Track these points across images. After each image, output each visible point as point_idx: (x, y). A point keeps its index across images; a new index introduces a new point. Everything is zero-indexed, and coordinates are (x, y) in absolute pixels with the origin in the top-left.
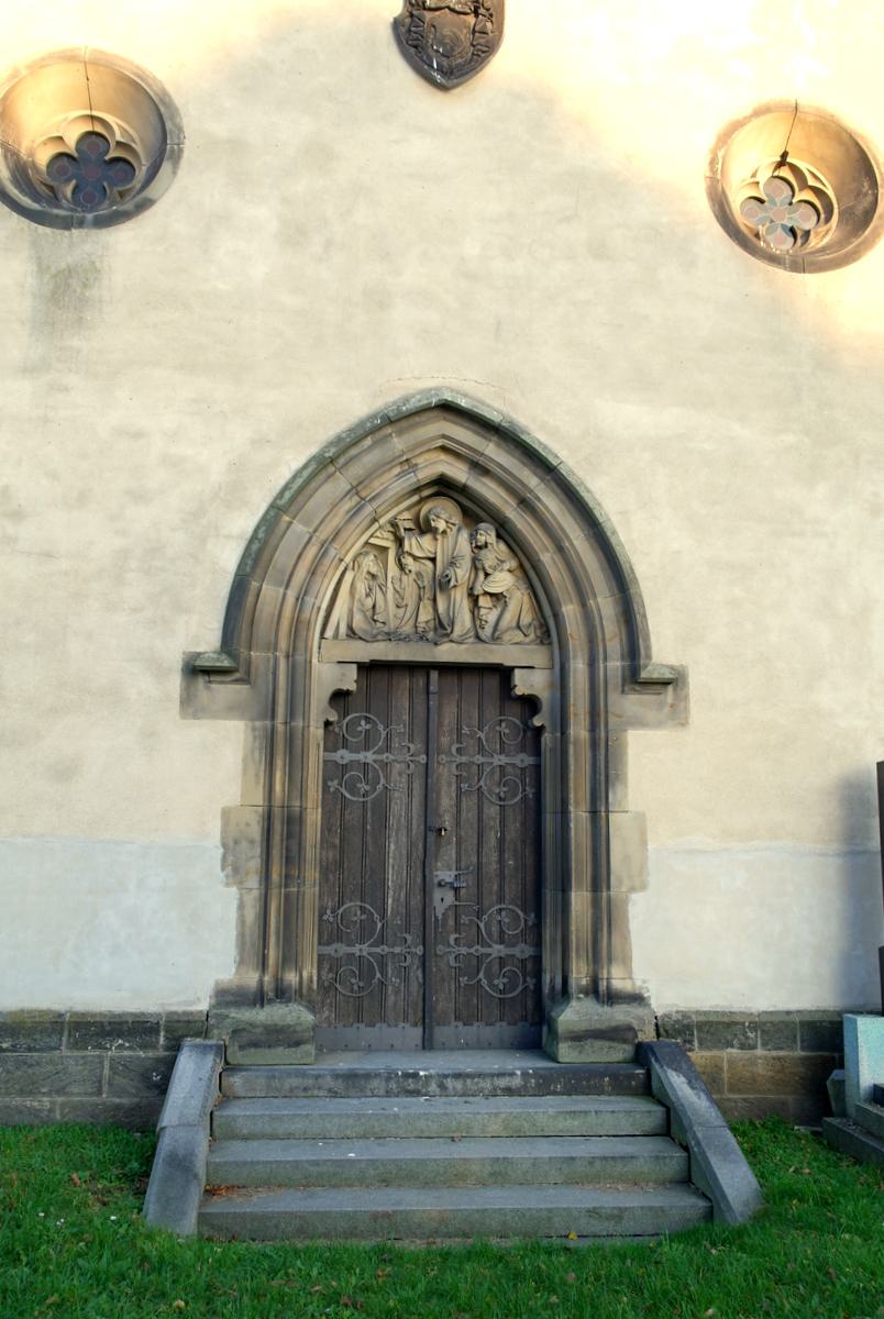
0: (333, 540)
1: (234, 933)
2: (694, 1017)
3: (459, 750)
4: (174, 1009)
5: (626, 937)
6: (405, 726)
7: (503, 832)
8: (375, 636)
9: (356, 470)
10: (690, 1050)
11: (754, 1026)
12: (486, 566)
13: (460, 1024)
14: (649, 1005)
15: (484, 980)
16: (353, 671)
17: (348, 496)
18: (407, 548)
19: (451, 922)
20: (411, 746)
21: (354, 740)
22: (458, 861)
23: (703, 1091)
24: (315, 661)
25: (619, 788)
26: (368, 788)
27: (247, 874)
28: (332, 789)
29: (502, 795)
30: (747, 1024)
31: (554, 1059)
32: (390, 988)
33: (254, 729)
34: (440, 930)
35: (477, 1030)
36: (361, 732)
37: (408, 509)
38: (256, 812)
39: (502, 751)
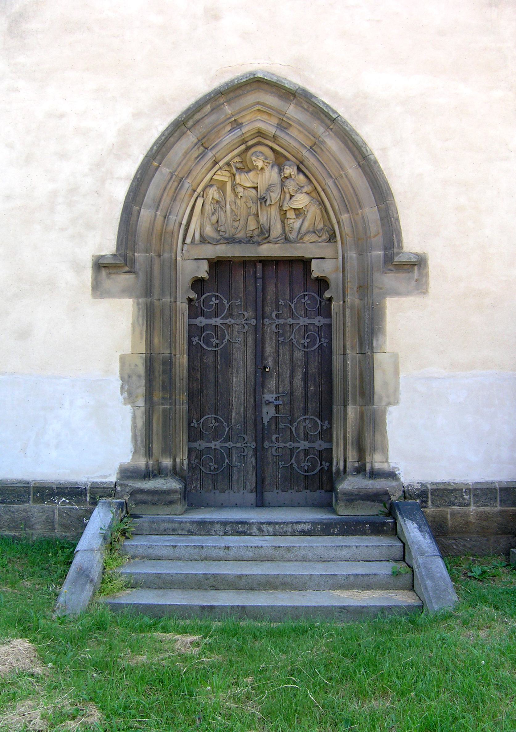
0: (187, 177)
1: (130, 434)
2: (428, 486)
3: (277, 316)
4: (95, 480)
5: (384, 435)
6: (241, 301)
7: (307, 369)
8: (218, 241)
9: (201, 129)
10: (425, 507)
11: (468, 491)
12: (291, 190)
13: (280, 491)
14: (399, 479)
15: (295, 464)
16: (205, 266)
17: (196, 147)
18: (238, 180)
19: (273, 427)
20: (245, 313)
21: (208, 311)
22: (278, 387)
23: (428, 533)
24: (179, 258)
25: (381, 337)
26: (218, 342)
27: (137, 396)
28: (194, 343)
29: (306, 344)
30: (464, 490)
31: (335, 512)
32: (235, 469)
33: (138, 304)
34: (266, 432)
35: (291, 495)
36: (213, 305)
37: (239, 155)
38: (141, 357)
39: (306, 315)
